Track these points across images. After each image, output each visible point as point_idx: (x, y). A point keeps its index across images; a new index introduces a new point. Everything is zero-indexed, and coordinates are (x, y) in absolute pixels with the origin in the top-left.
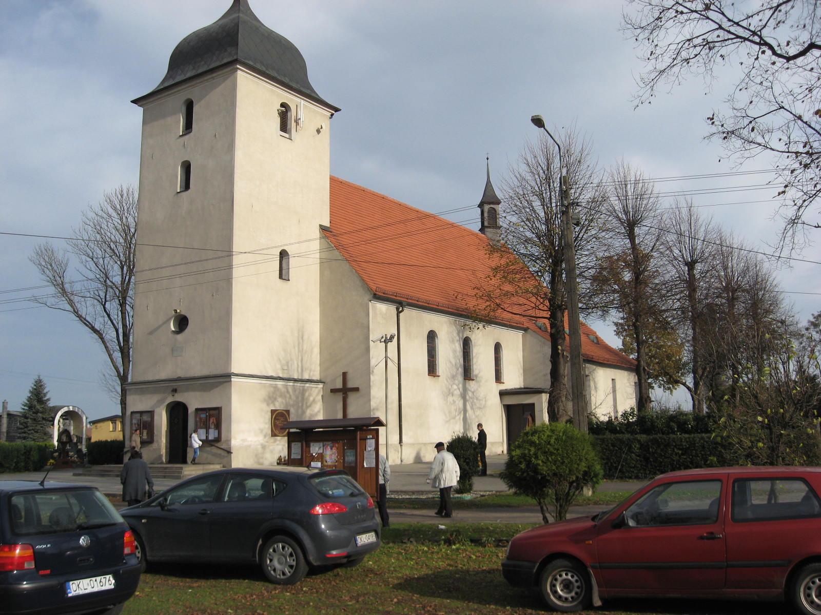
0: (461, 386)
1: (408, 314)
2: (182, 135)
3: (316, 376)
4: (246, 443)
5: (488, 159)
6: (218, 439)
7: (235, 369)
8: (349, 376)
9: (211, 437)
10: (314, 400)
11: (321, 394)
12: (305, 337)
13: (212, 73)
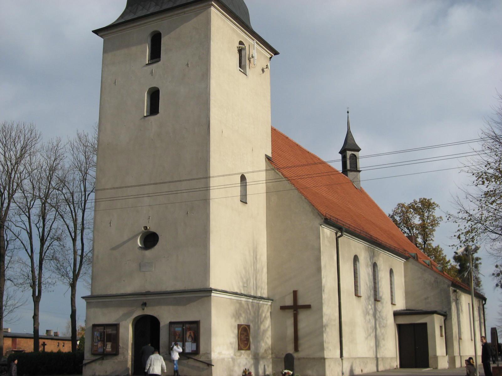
0: (373, 306)
1: (346, 239)
2: (149, 64)
3: (265, 295)
4: (221, 357)
5: (348, 112)
6: (196, 352)
7: (212, 286)
8: (299, 294)
9: (188, 350)
10: (265, 317)
11: (270, 310)
12: (258, 257)
13: (184, 8)
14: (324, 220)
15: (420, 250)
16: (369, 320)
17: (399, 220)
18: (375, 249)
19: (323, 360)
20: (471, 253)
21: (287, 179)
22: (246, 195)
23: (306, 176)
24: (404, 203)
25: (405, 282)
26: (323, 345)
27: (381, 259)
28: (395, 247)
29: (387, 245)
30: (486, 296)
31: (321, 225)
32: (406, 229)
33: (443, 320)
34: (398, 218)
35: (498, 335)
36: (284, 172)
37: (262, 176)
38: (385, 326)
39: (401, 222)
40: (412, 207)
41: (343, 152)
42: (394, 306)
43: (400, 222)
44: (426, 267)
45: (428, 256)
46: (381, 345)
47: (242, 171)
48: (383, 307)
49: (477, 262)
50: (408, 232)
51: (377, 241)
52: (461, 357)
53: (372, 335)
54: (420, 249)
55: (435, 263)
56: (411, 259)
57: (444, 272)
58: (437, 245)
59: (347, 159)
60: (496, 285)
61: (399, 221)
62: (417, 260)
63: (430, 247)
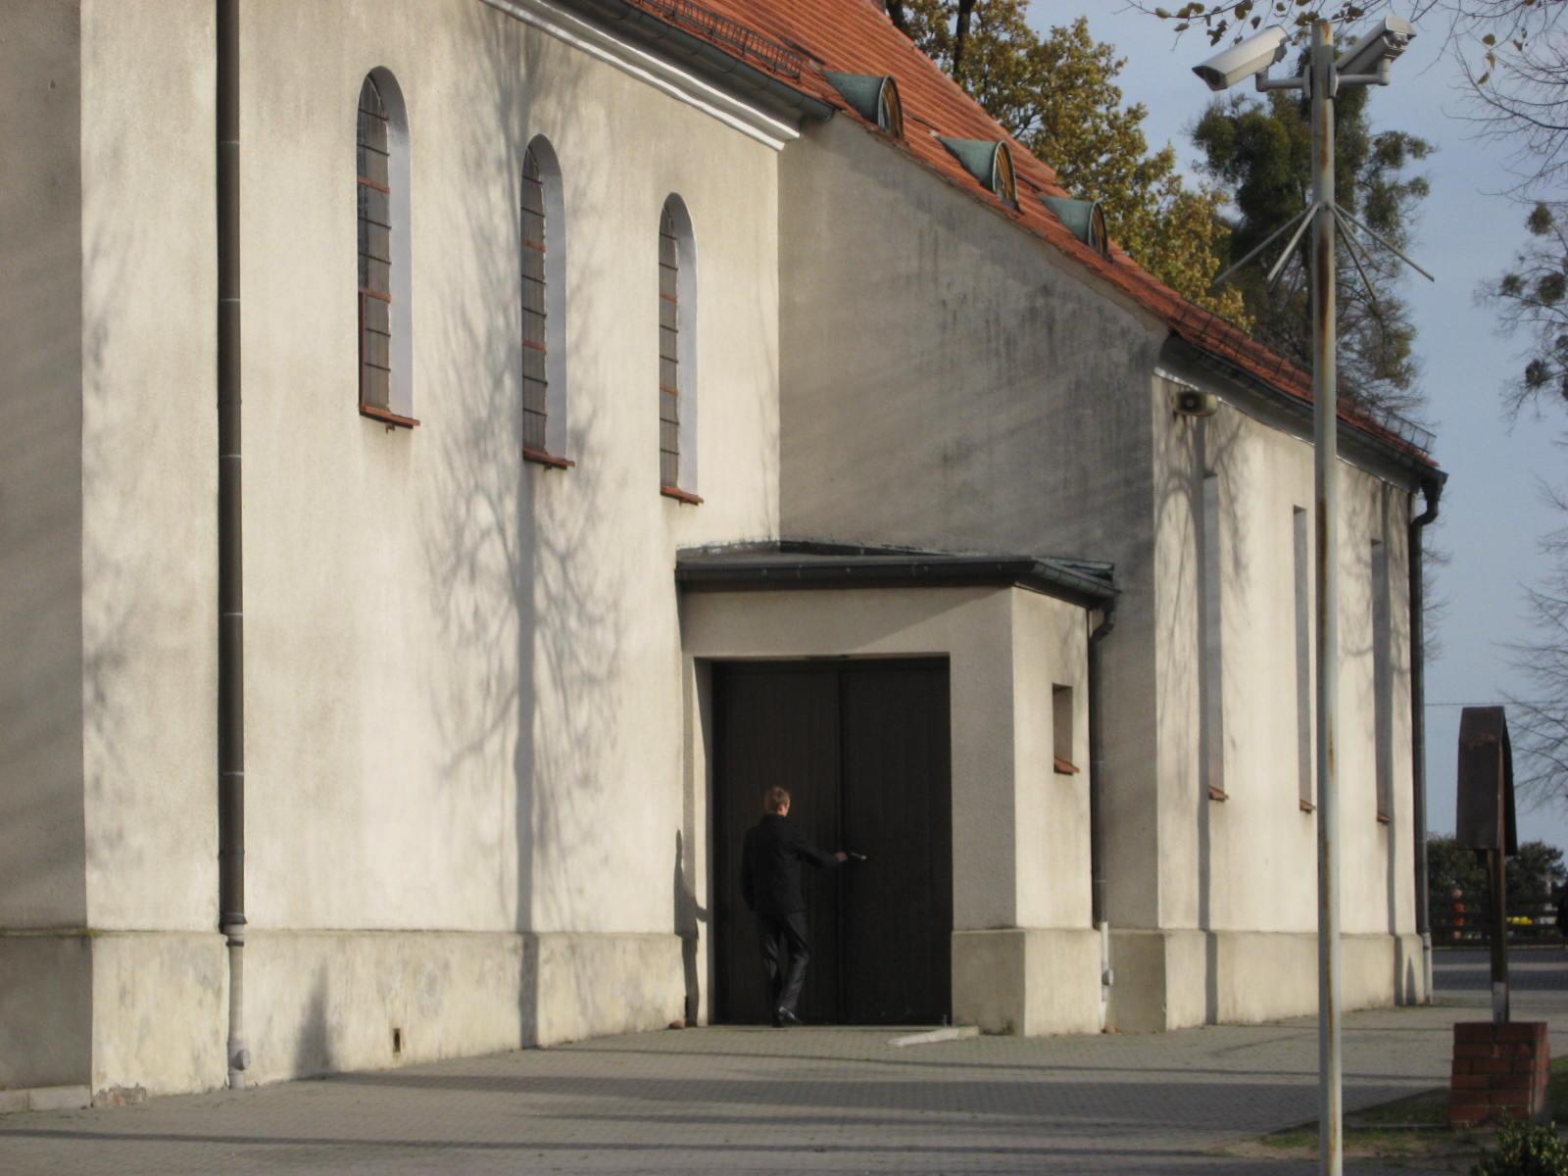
0: (510, 506)
15: (926, 58)
16: (470, 625)
18: (552, 28)
19: (70, 946)
20: (1337, 79)
25: (787, 311)
26: (75, 821)
27: (592, 111)
28: (716, 17)
30: (1441, 456)
33: (1080, 638)
35: (1520, 774)
38: (601, 671)
42: (687, 507)
44: (964, 190)
45: (993, 107)
46: (569, 833)
48: (592, 517)
49: (1388, 176)
52: (1212, 938)
53: (493, 745)
54: (923, 48)
55: (1046, 171)
56: (841, 125)
57: (1114, 245)
58: (1068, 23)
60: (1529, 371)
62: (893, 133)
63: (1004, 37)
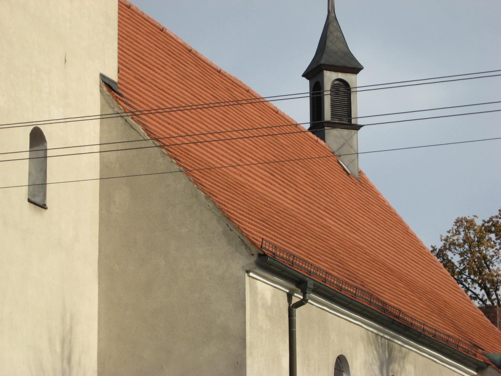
12: (75, 357)
14: (255, 258)
17: (460, 264)
21: (158, 144)
22: (44, 184)
23: (210, 135)
24: (472, 217)
28: (448, 336)
29: (427, 331)
31: (248, 272)
32: (478, 288)
34: (456, 259)
36: (153, 125)
37: (92, 132)
39: (464, 269)
40: (493, 229)
41: (314, 73)
43: (461, 268)
47: (35, 116)
50: (483, 295)
51: (398, 317)
59: (325, 93)
61: (458, 266)
